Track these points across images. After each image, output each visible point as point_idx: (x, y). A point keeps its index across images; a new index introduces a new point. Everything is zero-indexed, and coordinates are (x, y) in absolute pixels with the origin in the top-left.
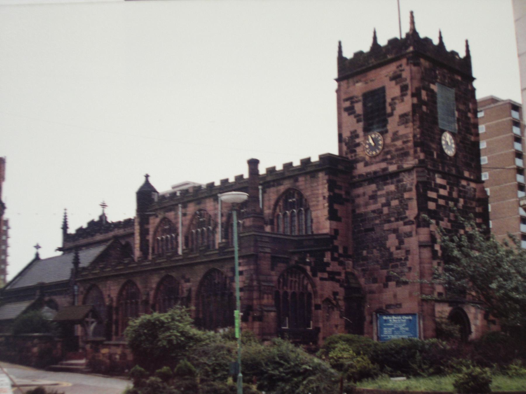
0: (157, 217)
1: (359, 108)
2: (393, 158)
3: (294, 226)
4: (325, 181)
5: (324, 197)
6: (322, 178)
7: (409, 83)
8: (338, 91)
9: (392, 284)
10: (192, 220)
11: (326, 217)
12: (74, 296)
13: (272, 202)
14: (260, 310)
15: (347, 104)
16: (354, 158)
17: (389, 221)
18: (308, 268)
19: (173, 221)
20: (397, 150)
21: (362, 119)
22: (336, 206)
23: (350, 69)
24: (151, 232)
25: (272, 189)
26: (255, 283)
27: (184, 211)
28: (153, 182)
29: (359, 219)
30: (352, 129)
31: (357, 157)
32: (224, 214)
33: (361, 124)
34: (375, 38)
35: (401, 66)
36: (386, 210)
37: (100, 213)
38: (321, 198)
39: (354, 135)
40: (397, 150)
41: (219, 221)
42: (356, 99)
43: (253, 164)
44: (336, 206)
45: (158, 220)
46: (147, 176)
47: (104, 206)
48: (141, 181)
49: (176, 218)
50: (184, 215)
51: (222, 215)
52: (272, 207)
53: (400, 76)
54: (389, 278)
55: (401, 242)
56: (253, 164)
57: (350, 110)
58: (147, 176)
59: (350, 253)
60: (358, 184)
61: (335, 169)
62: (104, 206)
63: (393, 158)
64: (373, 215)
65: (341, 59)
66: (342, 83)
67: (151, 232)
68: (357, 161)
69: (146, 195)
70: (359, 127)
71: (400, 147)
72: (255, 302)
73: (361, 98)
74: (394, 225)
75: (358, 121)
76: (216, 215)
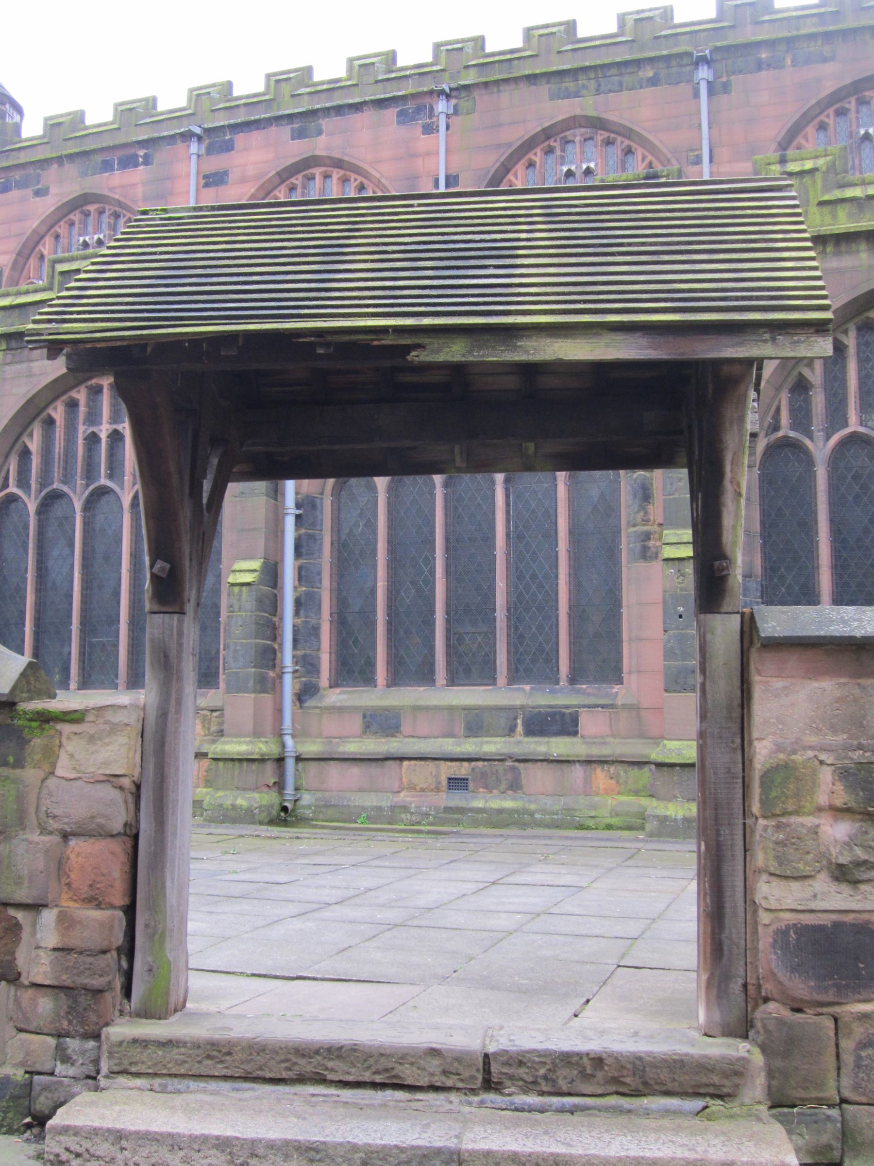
27: (216, 163)
45: (47, 205)
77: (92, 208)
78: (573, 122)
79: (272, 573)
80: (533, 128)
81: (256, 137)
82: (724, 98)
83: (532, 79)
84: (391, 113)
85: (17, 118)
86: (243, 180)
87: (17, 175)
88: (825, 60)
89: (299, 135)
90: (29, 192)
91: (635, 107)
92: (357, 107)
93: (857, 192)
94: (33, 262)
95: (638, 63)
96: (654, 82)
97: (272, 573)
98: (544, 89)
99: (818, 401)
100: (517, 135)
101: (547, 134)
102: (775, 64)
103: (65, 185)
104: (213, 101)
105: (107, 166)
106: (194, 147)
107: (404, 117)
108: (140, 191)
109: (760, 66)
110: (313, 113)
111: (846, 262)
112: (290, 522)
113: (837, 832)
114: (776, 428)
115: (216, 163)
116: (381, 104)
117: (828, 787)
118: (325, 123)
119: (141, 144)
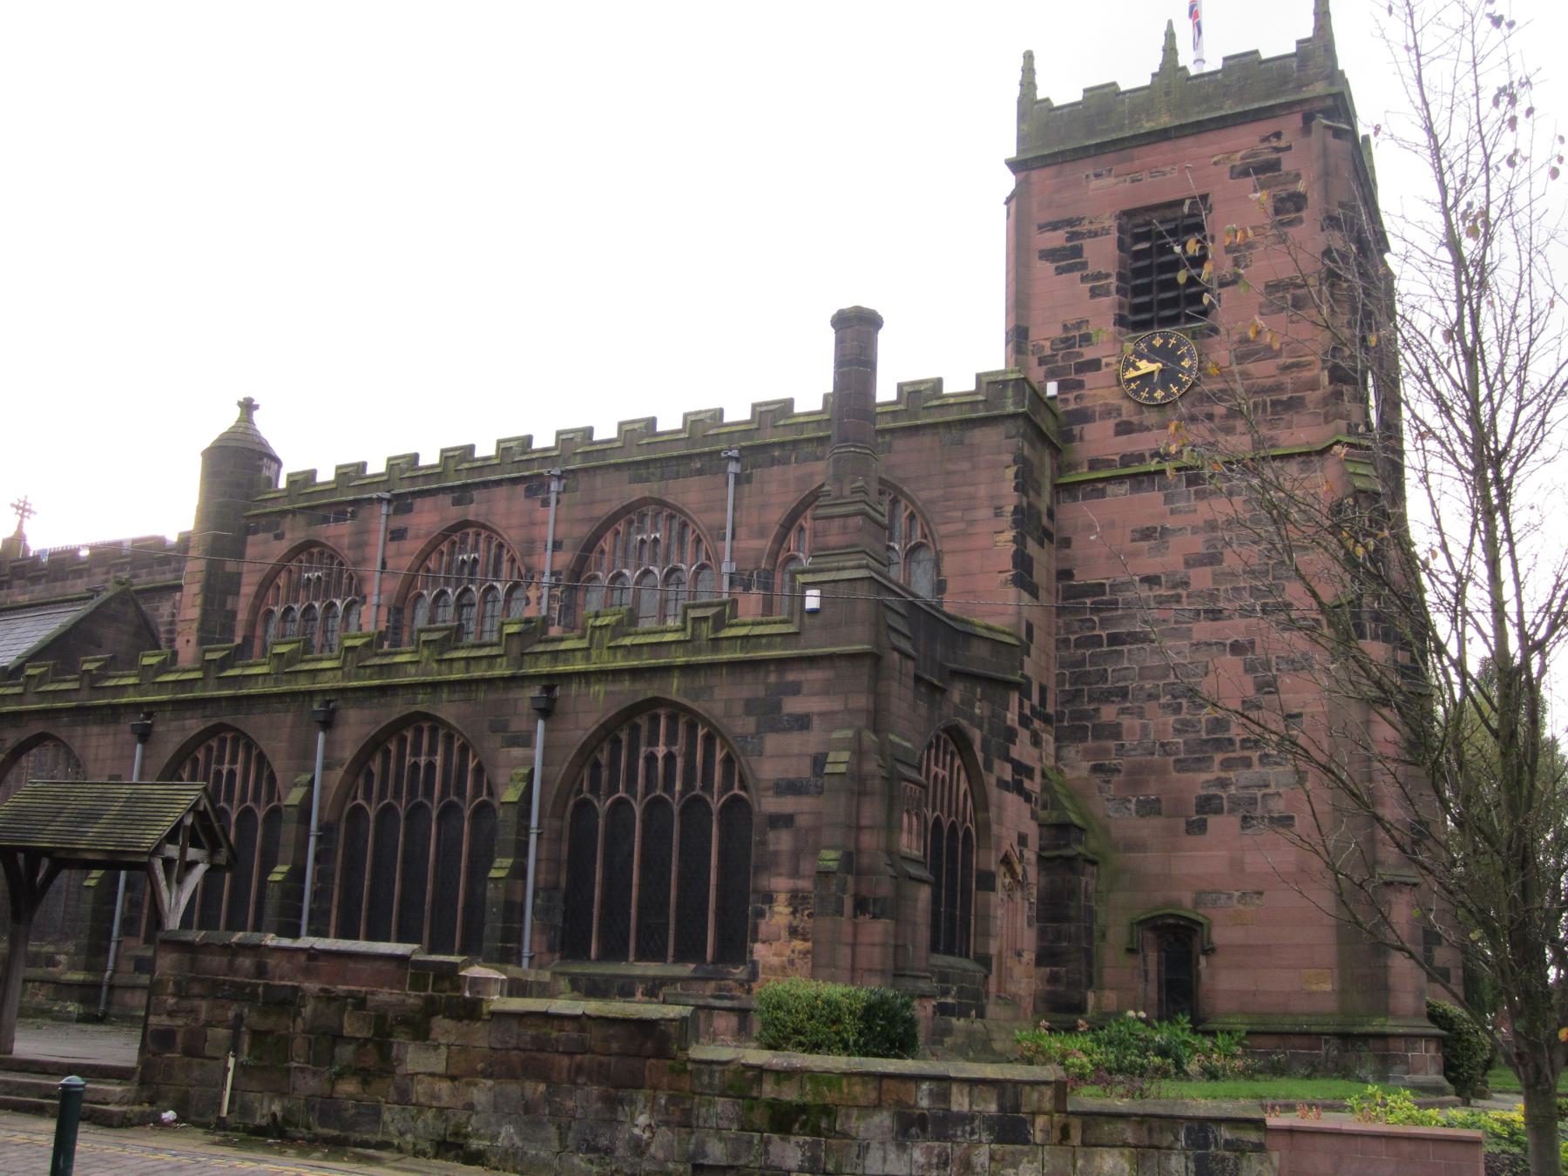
0: (279, 537)
1: (1103, 253)
2: (1234, 413)
3: (491, 667)
4: (1008, 458)
5: (998, 512)
6: (998, 446)
7: (1200, 229)
8: (1019, 202)
9: (1222, 825)
10: (424, 556)
11: (1008, 575)
12: (1372, 876)
13: (776, 516)
14: (890, 871)
15: (1057, 239)
16: (1072, 406)
17: (1215, 614)
18: (977, 736)
19: (348, 554)
20: (1253, 391)
21: (1113, 288)
22: (1032, 548)
23: (1063, 145)
24: (248, 589)
25: (859, 448)
26: (871, 766)
27: (399, 522)
28: (266, 426)
29: (1088, 601)
30: (1071, 319)
31: (1087, 403)
32: (567, 543)
33: (1108, 304)
34: (1170, 50)
35: (1278, 135)
36: (1201, 578)
37: (10, 532)
38: (984, 513)
39: (1075, 337)
40: (1253, 391)
41: (545, 561)
42: (1085, 227)
43: (857, 332)
44: (1032, 548)
45: (282, 547)
46: (248, 407)
47: (23, 509)
48: (229, 418)
49: (360, 545)
50: (397, 535)
51: (557, 546)
52: (774, 530)
53: (1274, 166)
54: (1208, 805)
55: (1267, 686)
56: (857, 332)
57: (1068, 258)
58: (248, 407)
59: (1050, 709)
60: (1094, 489)
61: (1028, 419)
62: (23, 509)
63: (1234, 413)
64: (1144, 592)
65: (1031, 109)
66: (1035, 175)
67: (248, 589)
68: (1083, 416)
69: (238, 463)
70: (1101, 315)
71: (1268, 382)
72: (868, 840)
73: (1110, 223)
74: (1235, 629)
75: (1094, 293)
76: (530, 546)
77: (315, 550)
78: (645, 501)
79: (297, 874)
80: (616, 505)
81: (428, 503)
82: (746, 488)
83: (617, 466)
84: (521, 489)
85: (274, 466)
86: (417, 537)
87: (264, 521)
88: (818, 459)
89: (457, 502)
90: (271, 535)
91: (688, 493)
92: (498, 483)
93: (627, 641)
94: (271, 592)
95: (690, 457)
96: (700, 472)
97: (297, 874)
98: (626, 475)
99: (605, 774)
100: (603, 510)
101: (627, 510)
102: (783, 461)
103: (295, 533)
104: (402, 471)
105: (326, 520)
106: (384, 509)
107: (530, 493)
108: (346, 541)
109: (773, 462)
110: (465, 487)
111: (617, 687)
112: (312, 840)
113: (171, 1001)
114: (580, 791)
115: (399, 522)
116: (514, 481)
117: (171, 988)
118: (476, 494)
119: (350, 503)
